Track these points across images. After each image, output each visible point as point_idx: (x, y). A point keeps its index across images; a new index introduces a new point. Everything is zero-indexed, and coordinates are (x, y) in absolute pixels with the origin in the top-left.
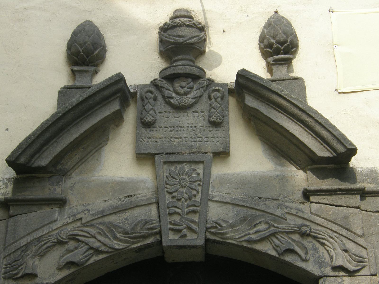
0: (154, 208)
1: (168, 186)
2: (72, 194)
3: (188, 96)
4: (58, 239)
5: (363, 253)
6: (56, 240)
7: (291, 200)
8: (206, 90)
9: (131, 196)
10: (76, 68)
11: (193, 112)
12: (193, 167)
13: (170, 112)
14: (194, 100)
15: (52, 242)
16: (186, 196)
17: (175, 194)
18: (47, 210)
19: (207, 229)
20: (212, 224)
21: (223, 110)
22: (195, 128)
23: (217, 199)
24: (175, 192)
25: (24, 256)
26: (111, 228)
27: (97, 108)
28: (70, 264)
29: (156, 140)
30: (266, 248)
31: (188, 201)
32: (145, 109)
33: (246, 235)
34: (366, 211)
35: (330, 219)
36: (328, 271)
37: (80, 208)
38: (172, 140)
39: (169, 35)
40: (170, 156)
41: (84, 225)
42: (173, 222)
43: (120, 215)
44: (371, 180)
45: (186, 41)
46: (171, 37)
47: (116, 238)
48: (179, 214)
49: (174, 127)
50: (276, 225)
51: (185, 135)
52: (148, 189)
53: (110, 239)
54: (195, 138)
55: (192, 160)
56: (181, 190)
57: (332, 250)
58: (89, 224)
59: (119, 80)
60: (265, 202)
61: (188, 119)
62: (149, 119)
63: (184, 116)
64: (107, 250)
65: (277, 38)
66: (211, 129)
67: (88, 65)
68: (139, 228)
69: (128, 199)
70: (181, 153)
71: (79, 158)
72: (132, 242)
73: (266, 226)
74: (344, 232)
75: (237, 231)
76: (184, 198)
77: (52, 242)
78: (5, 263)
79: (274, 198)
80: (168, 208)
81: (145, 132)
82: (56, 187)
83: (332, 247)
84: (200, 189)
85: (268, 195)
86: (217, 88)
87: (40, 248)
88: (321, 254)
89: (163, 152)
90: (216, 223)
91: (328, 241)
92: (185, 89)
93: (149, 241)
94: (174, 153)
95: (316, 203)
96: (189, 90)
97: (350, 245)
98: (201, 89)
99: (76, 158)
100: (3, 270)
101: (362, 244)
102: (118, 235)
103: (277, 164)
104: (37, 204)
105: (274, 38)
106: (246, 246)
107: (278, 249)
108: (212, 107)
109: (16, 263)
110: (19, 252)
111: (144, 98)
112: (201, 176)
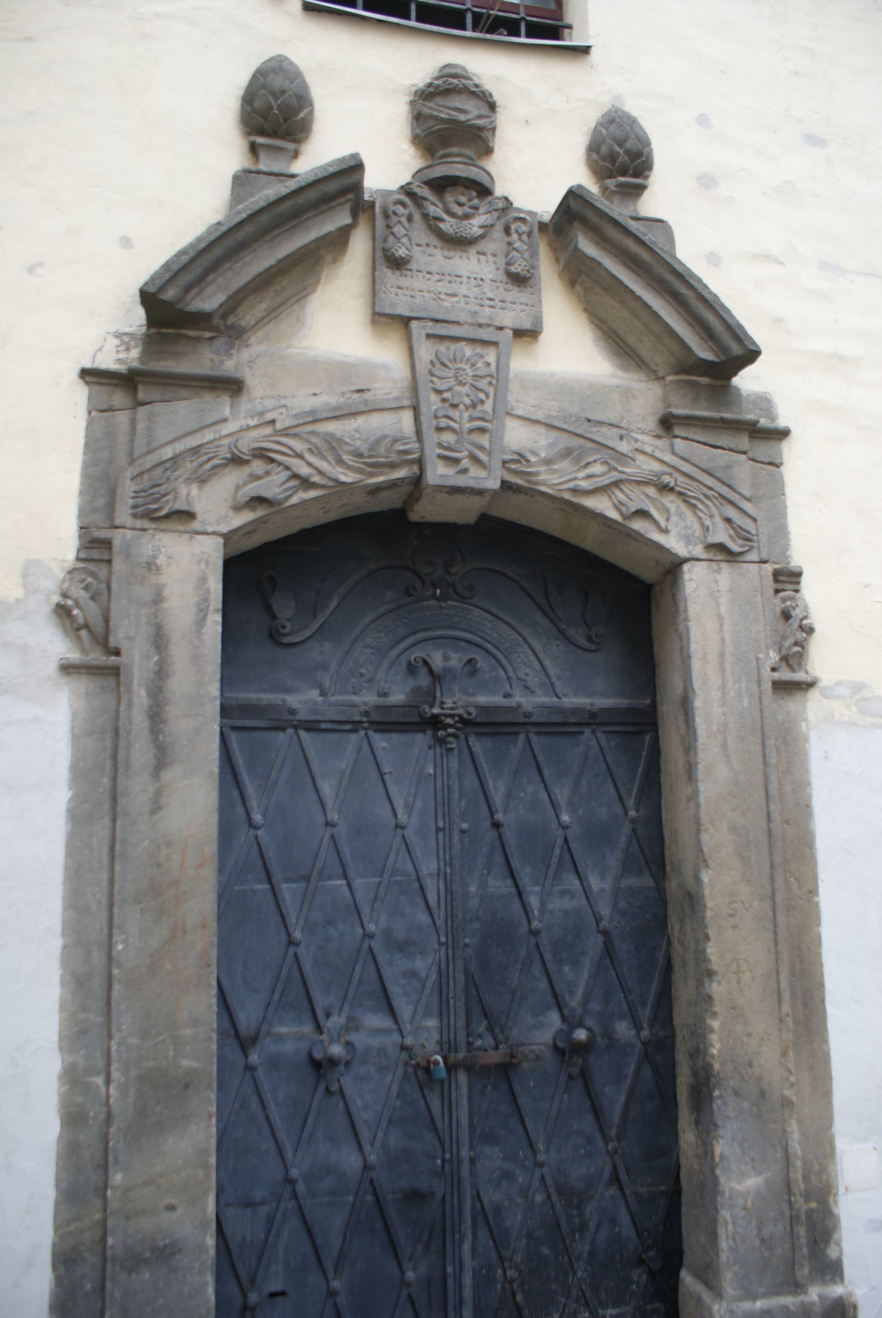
0: (406, 420)
1: (434, 379)
2: (253, 375)
4: (232, 453)
6: (228, 456)
10: (260, 140)
11: (478, 253)
12: (479, 350)
13: (435, 247)
14: (481, 231)
15: (223, 459)
16: (467, 401)
22: (481, 283)
23: (519, 412)
25: (172, 478)
26: (333, 444)
27: (309, 215)
28: (259, 501)
29: (412, 293)
32: (392, 233)
35: (704, 467)
36: (698, 551)
37: (269, 403)
38: (442, 296)
39: (438, 105)
40: (439, 325)
41: (277, 433)
44: (762, 413)
45: (470, 120)
46: (441, 109)
47: (340, 462)
49: (443, 275)
50: (620, 468)
52: (395, 382)
54: (482, 299)
56: (458, 388)
58: (286, 432)
59: (353, 169)
61: (466, 264)
62: (402, 252)
63: (461, 257)
64: (324, 482)
65: (628, 145)
66: (510, 287)
67: (282, 138)
68: (382, 450)
69: (356, 395)
70: (458, 323)
71: (265, 310)
72: (369, 472)
73: (605, 469)
74: (725, 491)
76: (465, 405)
78: (133, 488)
80: (436, 417)
81: (390, 277)
82: (225, 358)
84: (491, 391)
86: (522, 215)
87: (201, 465)
88: (688, 523)
93: (401, 473)
95: (683, 438)
96: (472, 211)
97: (732, 513)
98: (493, 213)
99: (260, 309)
102: (345, 457)
104: (190, 386)
105: (620, 145)
106: (568, 500)
107: (624, 509)
108: (514, 249)
109: (156, 490)
110: (159, 471)
111: (391, 213)
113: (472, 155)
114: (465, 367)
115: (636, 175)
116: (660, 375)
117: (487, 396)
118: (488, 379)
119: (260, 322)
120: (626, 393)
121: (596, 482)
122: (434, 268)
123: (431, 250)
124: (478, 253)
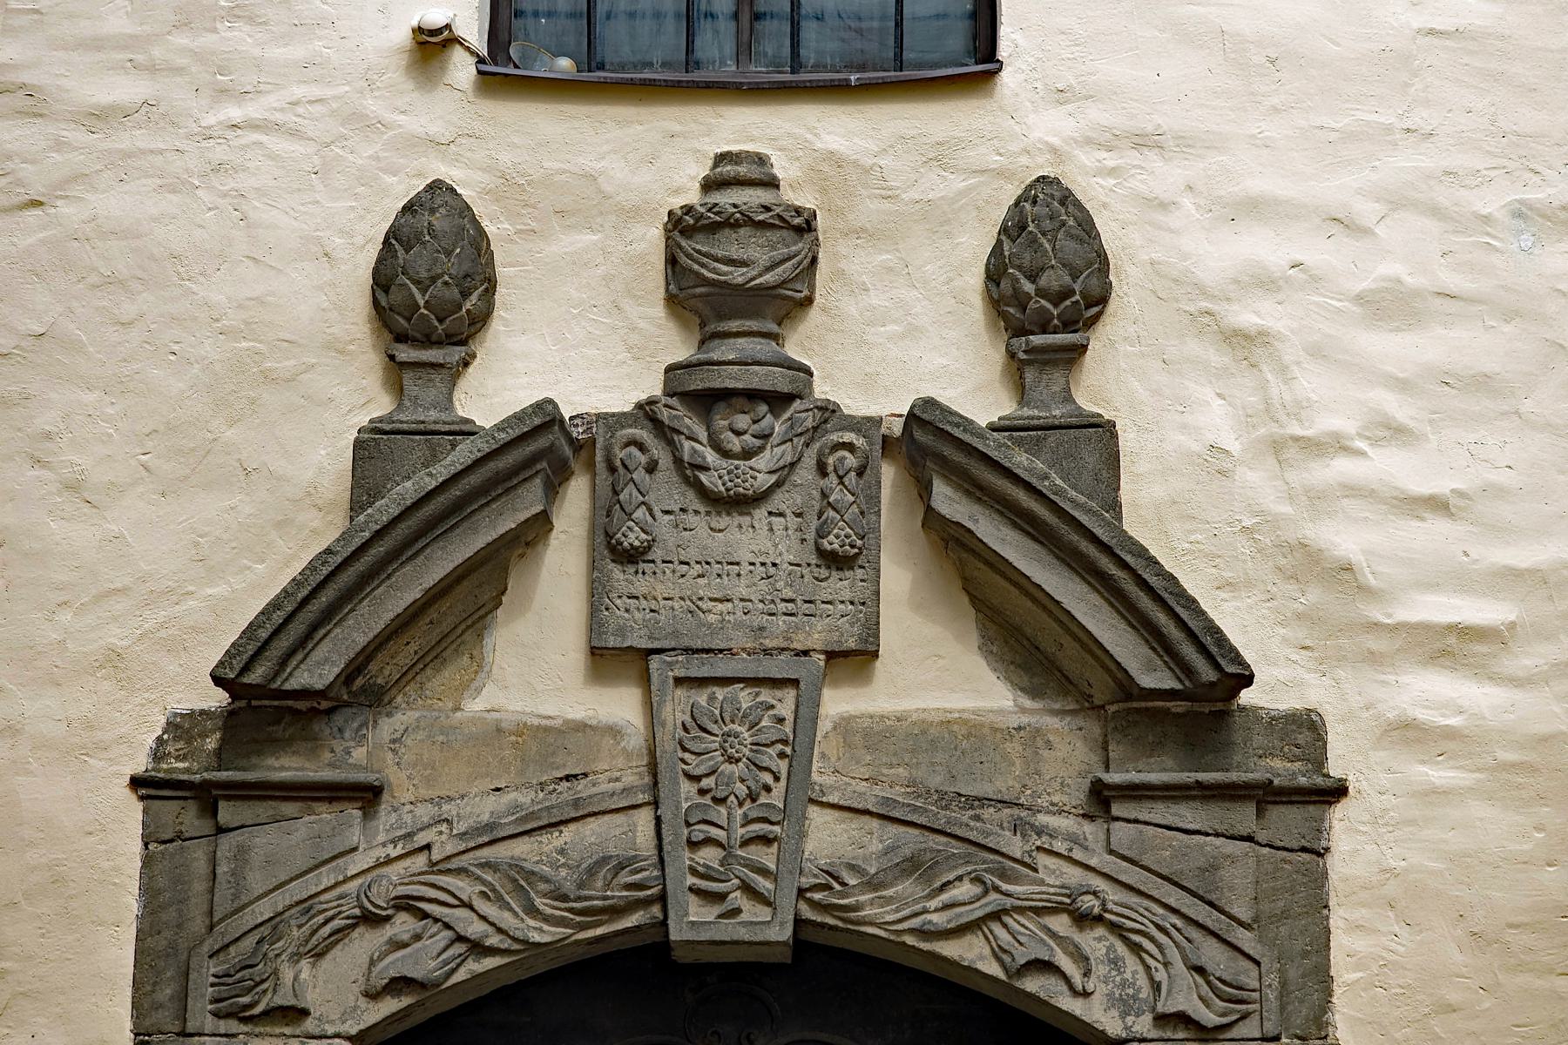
0: (644, 819)
1: (687, 756)
3: (752, 462)
4: (361, 907)
5: (1250, 978)
6: (357, 912)
7: (1053, 804)
8: (812, 439)
9: (575, 776)
10: (405, 353)
12: (766, 695)
13: (696, 512)
14: (774, 478)
15: (348, 918)
16: (741, 790)
17: (707, 783)
18: (325, 814)
19: (801, 892)
20: (815, 876)
21: (862, 513)
22: (772, 570)
23: (833, 798)
24: (707, 775)
25: (271, 955)
26: (521, 879)
28: (399, 984)
30: (972, 952)
31: (748, 805)
33: (916, 915)
34: (1271, 847)
35: (1165, 871)
42: (700, 869)
43: (544, 838)
47: (532, 911)
48: (720, 844)
50: (1005, 887)
51: (745, 593)
53: (516, 914)
55: (761, 675)
56: (727, 768)
57: (1160, 966)
60: (978, 811)
61: (750, 538)
62: (634, 538)
66: (824, 573)
73: (977, 890)
75: (889, 900)
77: (348, 918)
78: (212, 970)
79: (1006, 798)
80: (688, 824)
81: (619, 575)
83: (1159, 957)
84: (783, 766)
85: (986, 789)
86: (849, 437)
88: (1128, 975)
89: (673, 644)
90: (827, 872)
91: (1152, 939)
92: (747, 437)
94: (708, 651)
95: (1128, 821)
96: (758, 442)
97: (1212, 955)
98: (795, 440)
100: (211, 989)
101: (1246, 950)
102: (539, 902)
103: (1022, 689)
109: (246, 973)
111: (618, 463)
112: (788, 728)
113: (773, 327)
114: (739, 729)
115: (1069, 325)
116: (1097, 702)
117: (777, 779)
118: (780, 746)
119: (409, 674)
120: (1033, 737)
121: (960, 915)
122: (692, 554)
123: (691, 519)
124: (770, 513)
